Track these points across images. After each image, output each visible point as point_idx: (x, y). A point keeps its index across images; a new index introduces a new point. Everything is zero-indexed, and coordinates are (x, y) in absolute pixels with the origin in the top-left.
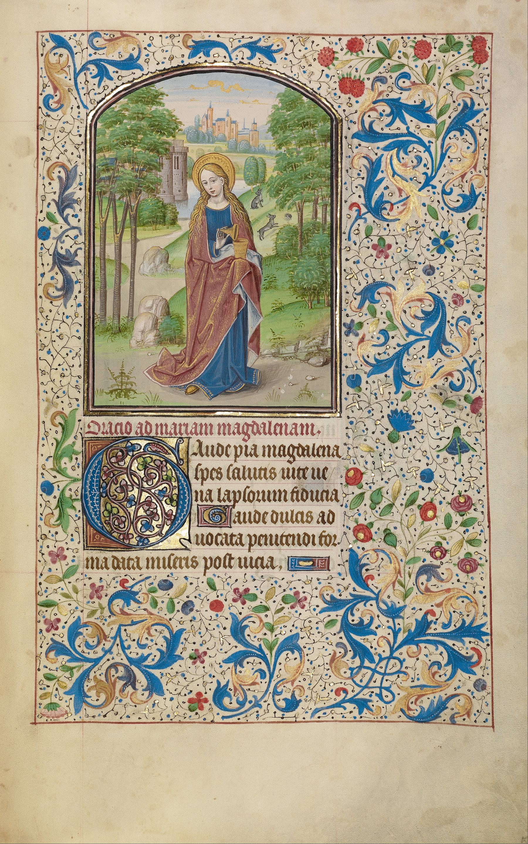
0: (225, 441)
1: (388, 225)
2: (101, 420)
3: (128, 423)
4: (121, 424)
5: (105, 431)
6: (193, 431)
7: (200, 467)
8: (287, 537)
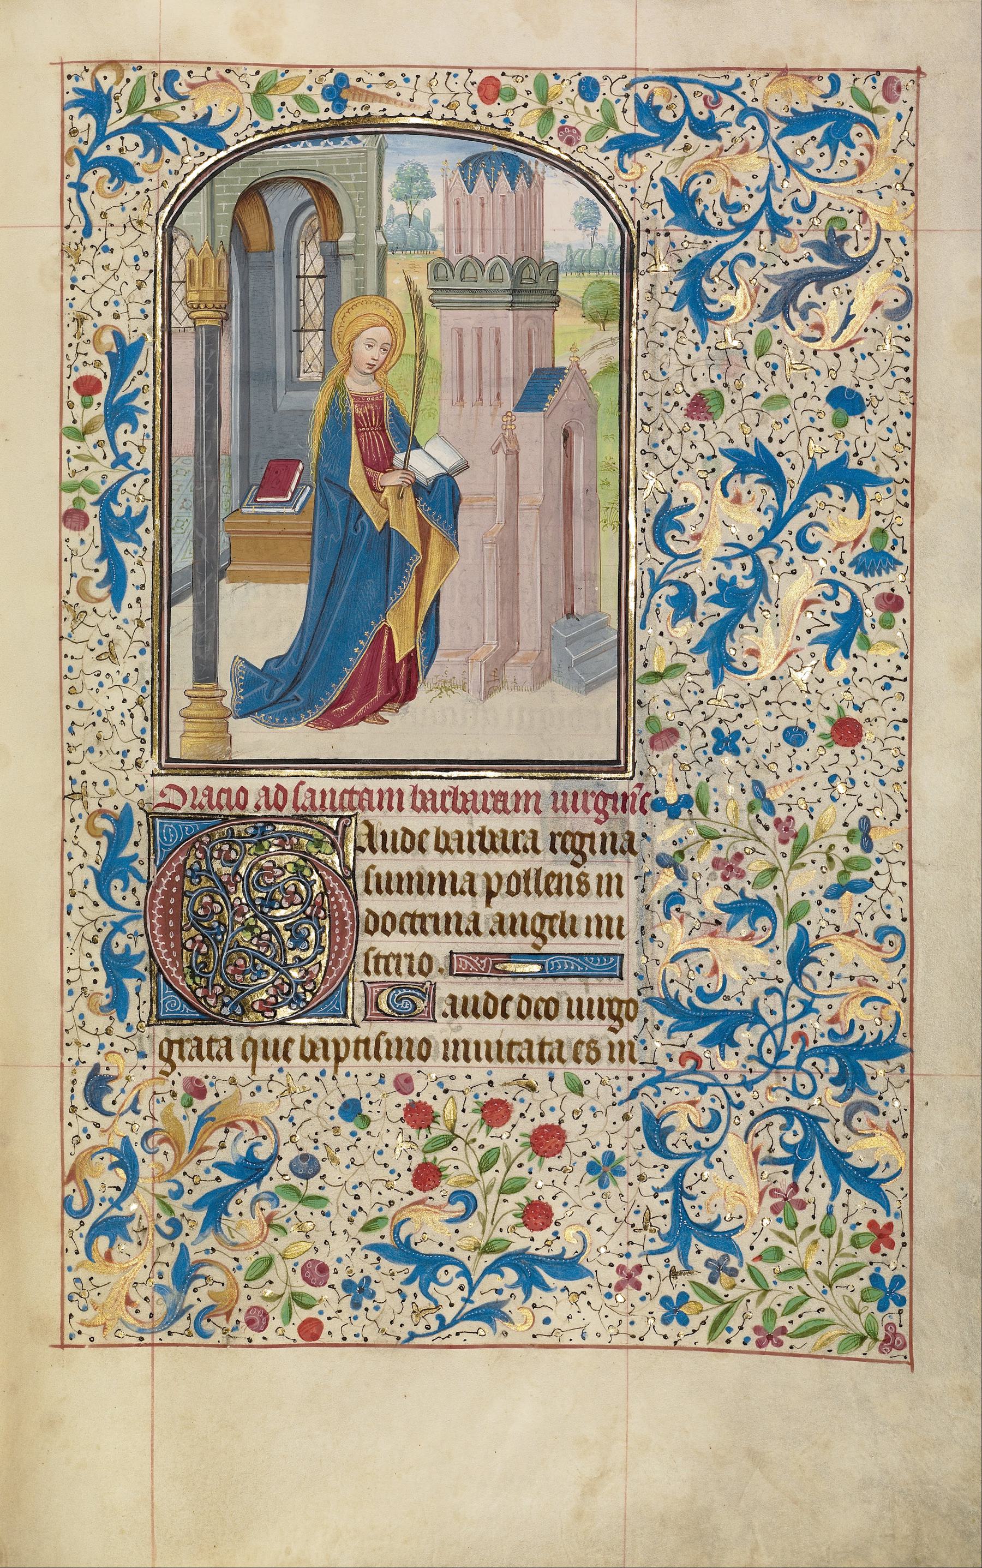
0: (417, 823)
2: (186, 782)
3: (242, 789)
5: (196, 803)
6: (307, 804)
7: (383, 1039)
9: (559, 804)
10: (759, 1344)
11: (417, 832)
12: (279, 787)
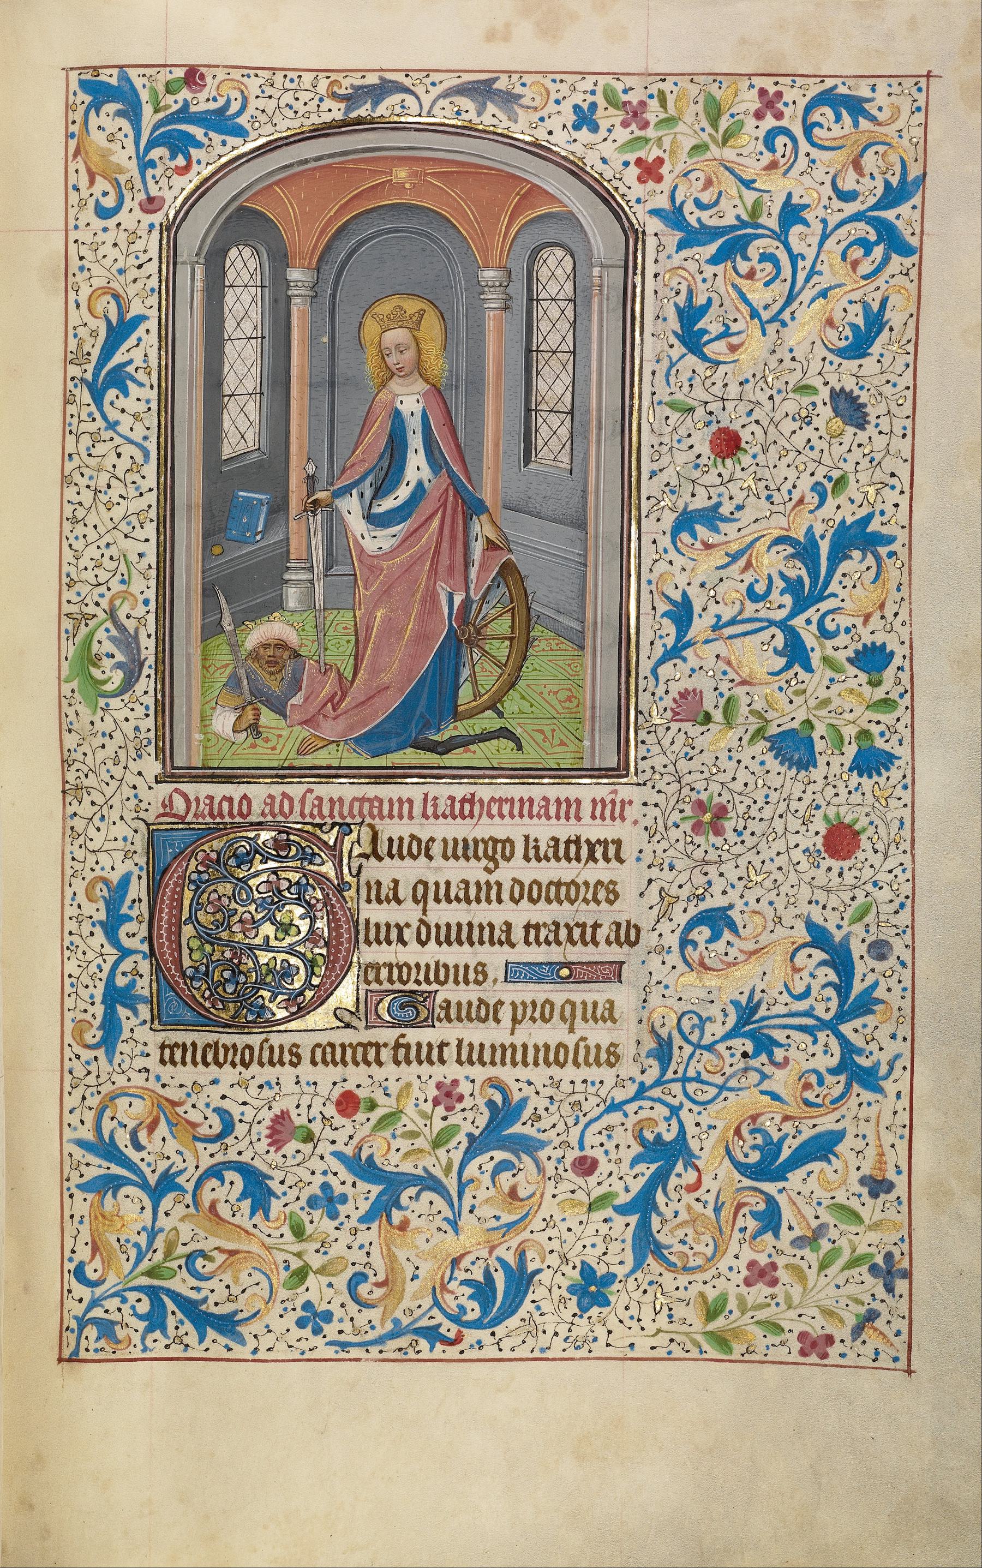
1: (905, 852)
3: (245, 797)
4: (230, 800)
7: (582, 1044)
8: (172, 1048)
9: (406, 806)
10: (803, 1353)
11: (424, 838)
12: (284, 795)
